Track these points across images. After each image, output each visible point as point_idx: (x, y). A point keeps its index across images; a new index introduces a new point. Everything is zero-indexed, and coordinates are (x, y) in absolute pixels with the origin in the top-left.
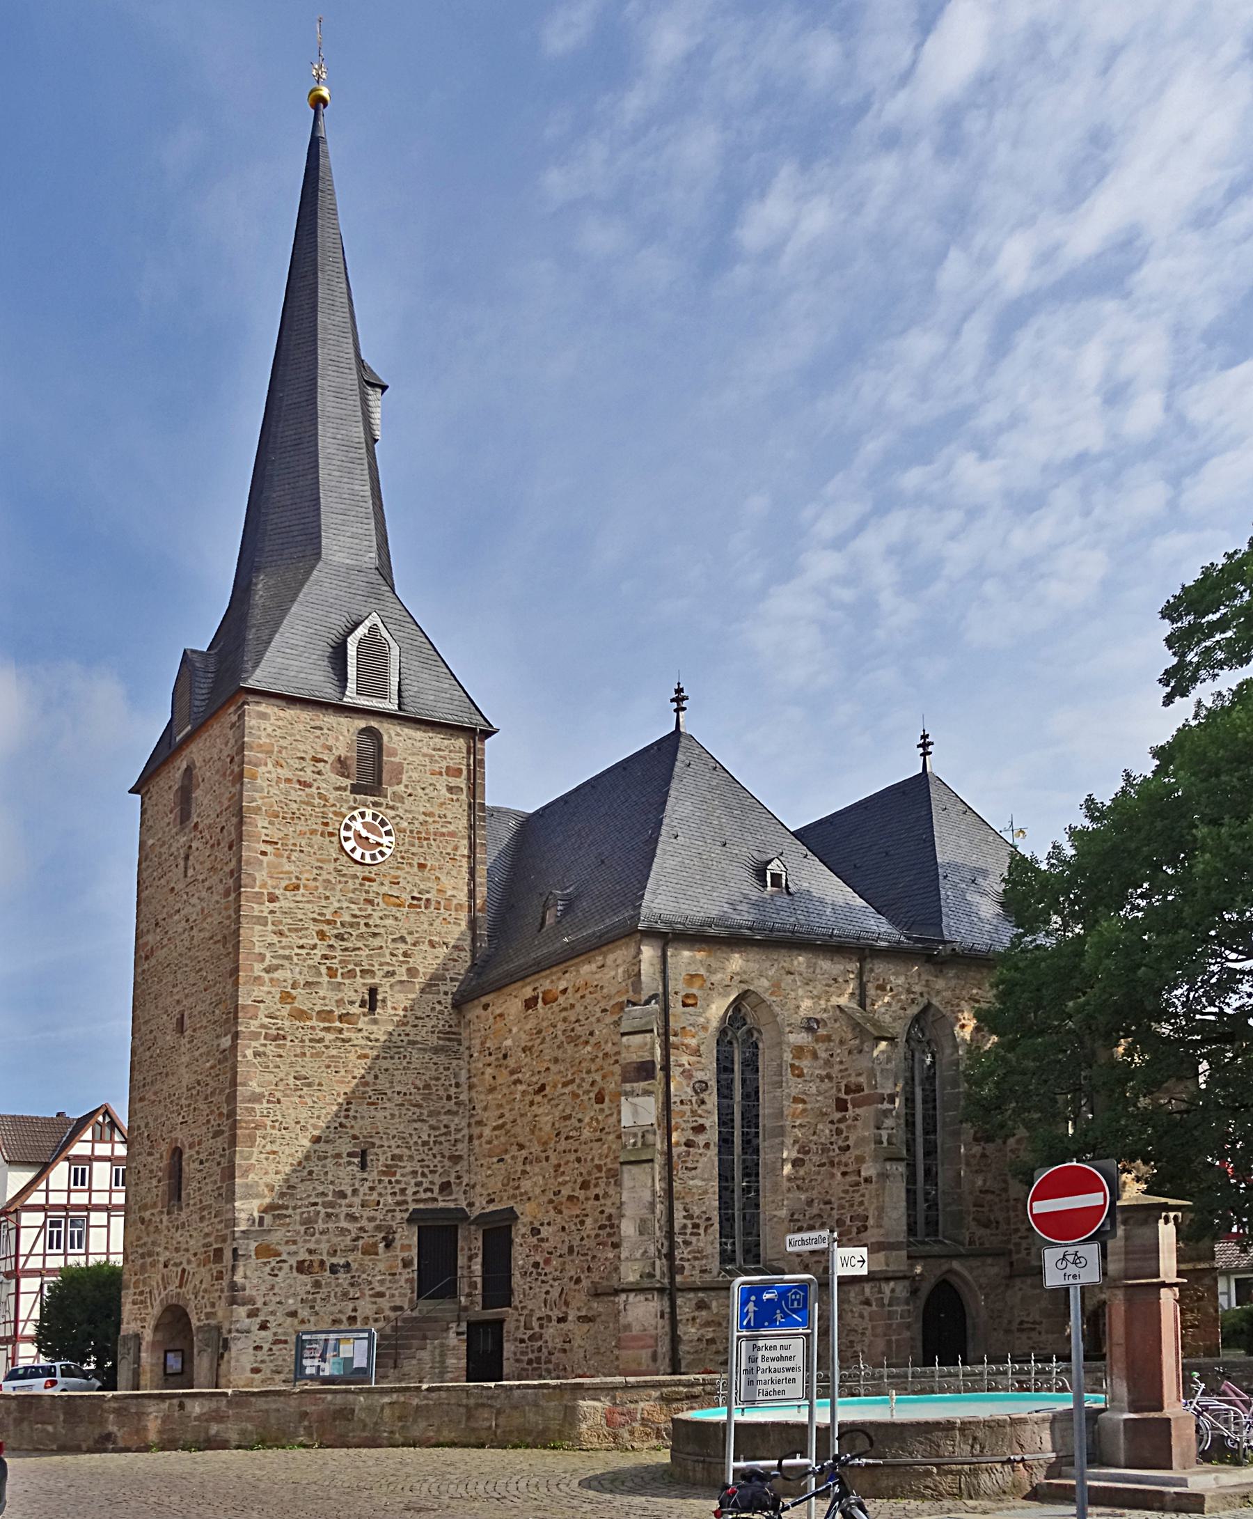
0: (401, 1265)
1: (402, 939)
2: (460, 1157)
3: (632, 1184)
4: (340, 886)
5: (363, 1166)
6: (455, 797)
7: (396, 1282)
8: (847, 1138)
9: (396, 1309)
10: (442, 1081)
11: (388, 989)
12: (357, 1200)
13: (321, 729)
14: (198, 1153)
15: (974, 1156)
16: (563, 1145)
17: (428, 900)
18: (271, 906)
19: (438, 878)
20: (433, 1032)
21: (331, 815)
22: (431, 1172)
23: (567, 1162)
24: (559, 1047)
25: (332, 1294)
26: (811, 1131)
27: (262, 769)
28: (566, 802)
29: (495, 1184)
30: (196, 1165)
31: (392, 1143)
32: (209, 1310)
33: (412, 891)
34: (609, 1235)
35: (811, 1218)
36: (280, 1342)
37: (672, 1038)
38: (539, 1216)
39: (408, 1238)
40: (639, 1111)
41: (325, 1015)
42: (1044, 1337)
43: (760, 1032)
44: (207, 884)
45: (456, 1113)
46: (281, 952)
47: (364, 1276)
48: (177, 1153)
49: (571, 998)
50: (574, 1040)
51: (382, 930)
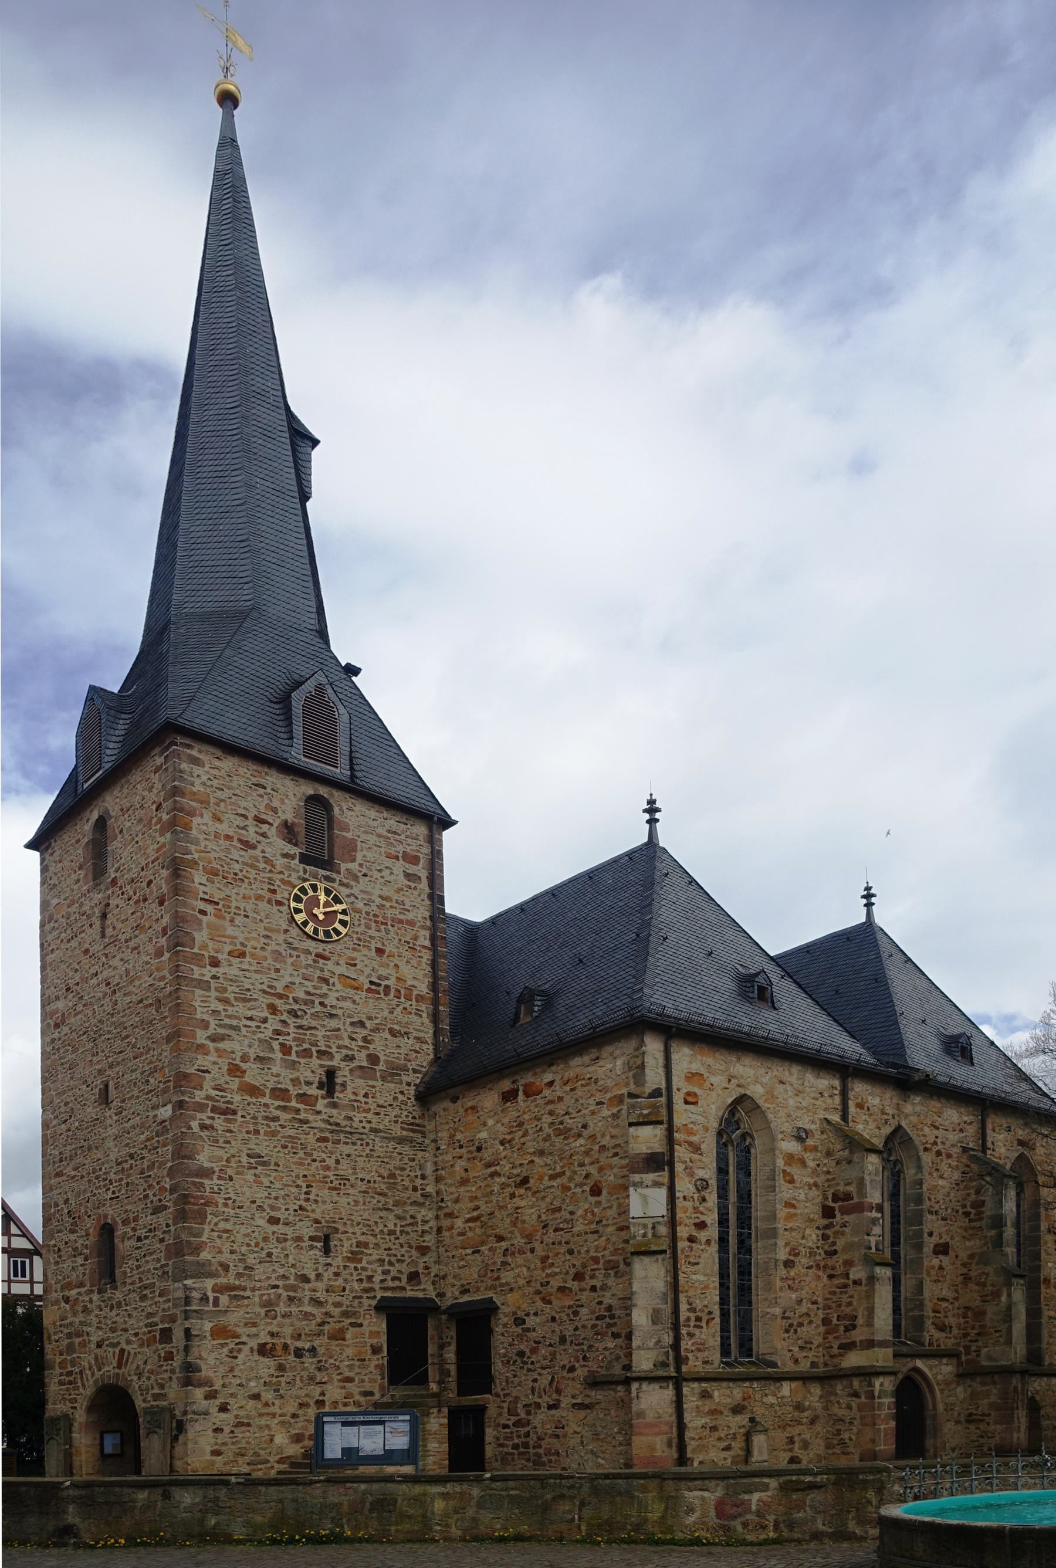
0: (369, 1351)
1: (362, 1024)
2: (427, 1248)
3: (643, 1274)
4: (290, 960)
5: (327, 1251)
6: (413, 885)
7: (365, 1367)
8: (834, 1244)
9: (366, 1394)
10: (407, 1172)
11: (347, 1073)
12: (321, 1285)
13: (265, 788)
14: (134, 1229)
15: (933, 1267)
16: (551, 1236)
17: (387, 987)
18: (214, 970)
19: (396, 966)
21: (278, 883)
22: (398, 1261)
24: (545, 1140)
25: (298, 1379)
26: (801, 1235)
27: (196, 820)
28: (522, 910)
29: (472, 1274)
30: (133, 1242)
31: (357, 1229)
32: (156, 1391)
33: (369, 975)
34: (609, 1326)
35: (800, 1317)
36: (242, 1424)
37: (676, 1134)
39: (376, 1327)
40: (647, 1202)
41: (280, 1093)
43: (753, 1138)
44: (132, 944)
45: (422, 1205)
46: (227, 1021)
47: (332, 1361)
48: (107, 1231)
49: (558, 1091)
50: (565, 1133)
51: (339, 1012)
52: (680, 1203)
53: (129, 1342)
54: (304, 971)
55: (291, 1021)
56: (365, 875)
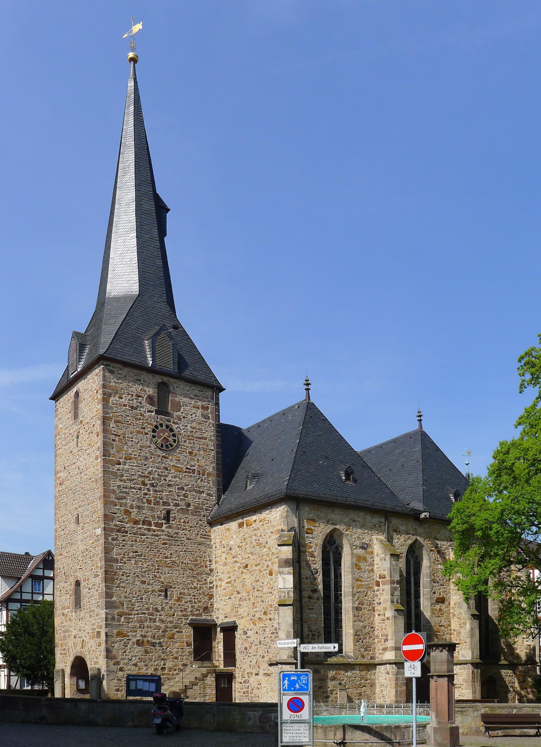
0: (185, 645)
1: (183, 489)
5: (166, 596)
8: (380, 599)
14: (87, 584)
20: (198, 534)
22: (199, 601)
23: (258, 602)
29: (228, 609)
30: (87, 590)
32: (95, 660)
38: (247, 626)
39: (188, 632)
42: (464, 691)
44: (88, 452)
46: (124, 490)
48: (78, 583)
50: (259, 545)
52: (304, 581)
53: (85, 637)
54: (157, 465)
55: (151, 488)
56: (184, 417)
